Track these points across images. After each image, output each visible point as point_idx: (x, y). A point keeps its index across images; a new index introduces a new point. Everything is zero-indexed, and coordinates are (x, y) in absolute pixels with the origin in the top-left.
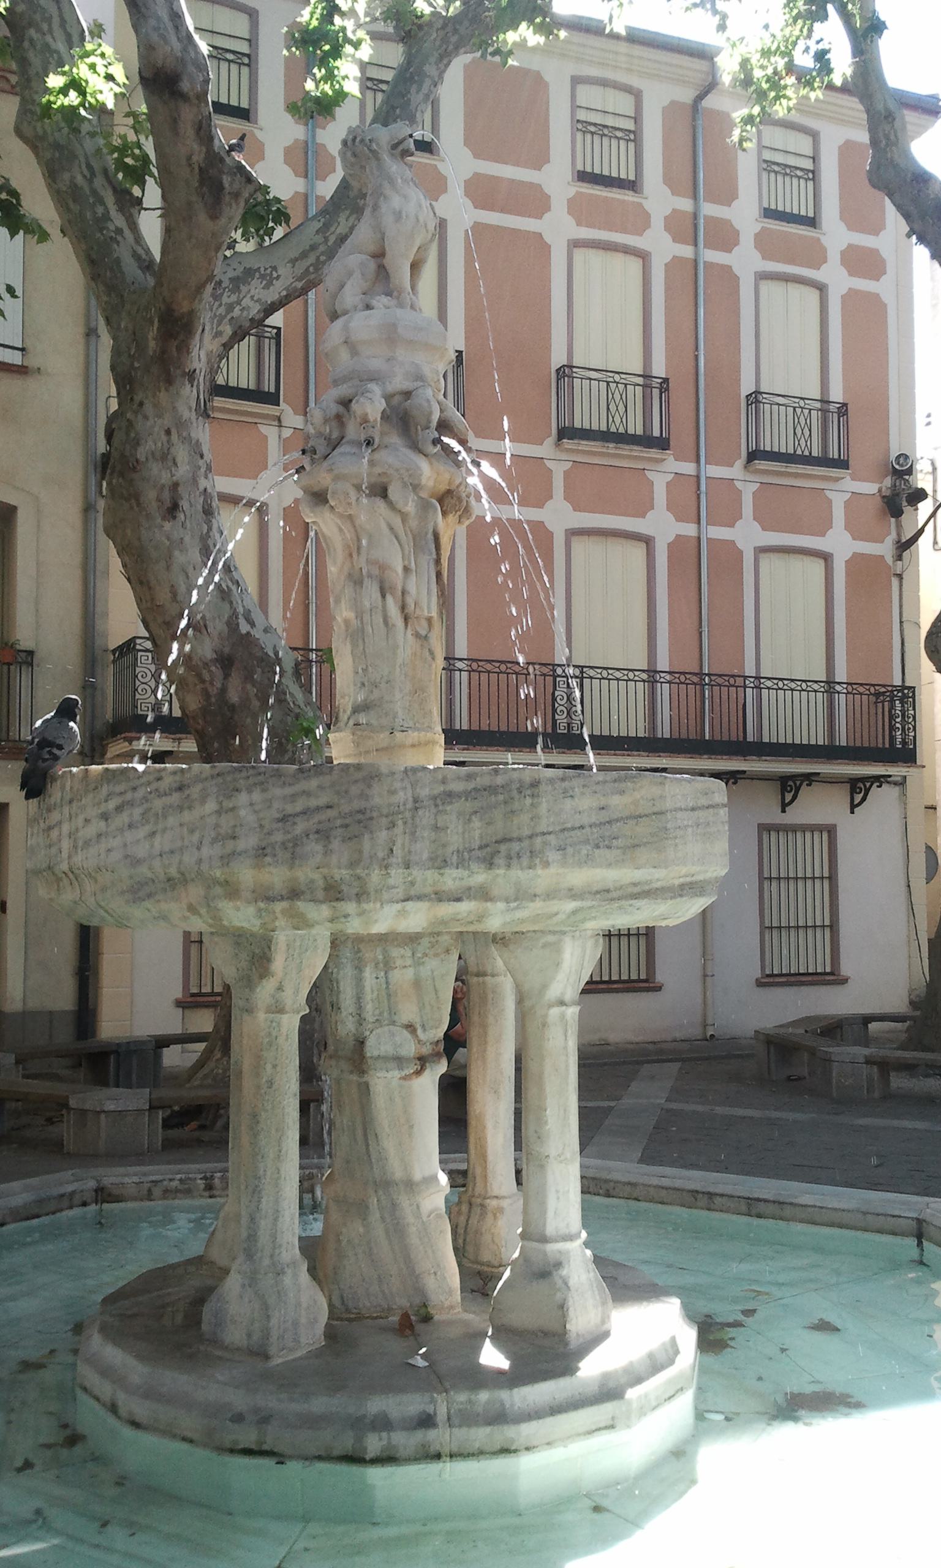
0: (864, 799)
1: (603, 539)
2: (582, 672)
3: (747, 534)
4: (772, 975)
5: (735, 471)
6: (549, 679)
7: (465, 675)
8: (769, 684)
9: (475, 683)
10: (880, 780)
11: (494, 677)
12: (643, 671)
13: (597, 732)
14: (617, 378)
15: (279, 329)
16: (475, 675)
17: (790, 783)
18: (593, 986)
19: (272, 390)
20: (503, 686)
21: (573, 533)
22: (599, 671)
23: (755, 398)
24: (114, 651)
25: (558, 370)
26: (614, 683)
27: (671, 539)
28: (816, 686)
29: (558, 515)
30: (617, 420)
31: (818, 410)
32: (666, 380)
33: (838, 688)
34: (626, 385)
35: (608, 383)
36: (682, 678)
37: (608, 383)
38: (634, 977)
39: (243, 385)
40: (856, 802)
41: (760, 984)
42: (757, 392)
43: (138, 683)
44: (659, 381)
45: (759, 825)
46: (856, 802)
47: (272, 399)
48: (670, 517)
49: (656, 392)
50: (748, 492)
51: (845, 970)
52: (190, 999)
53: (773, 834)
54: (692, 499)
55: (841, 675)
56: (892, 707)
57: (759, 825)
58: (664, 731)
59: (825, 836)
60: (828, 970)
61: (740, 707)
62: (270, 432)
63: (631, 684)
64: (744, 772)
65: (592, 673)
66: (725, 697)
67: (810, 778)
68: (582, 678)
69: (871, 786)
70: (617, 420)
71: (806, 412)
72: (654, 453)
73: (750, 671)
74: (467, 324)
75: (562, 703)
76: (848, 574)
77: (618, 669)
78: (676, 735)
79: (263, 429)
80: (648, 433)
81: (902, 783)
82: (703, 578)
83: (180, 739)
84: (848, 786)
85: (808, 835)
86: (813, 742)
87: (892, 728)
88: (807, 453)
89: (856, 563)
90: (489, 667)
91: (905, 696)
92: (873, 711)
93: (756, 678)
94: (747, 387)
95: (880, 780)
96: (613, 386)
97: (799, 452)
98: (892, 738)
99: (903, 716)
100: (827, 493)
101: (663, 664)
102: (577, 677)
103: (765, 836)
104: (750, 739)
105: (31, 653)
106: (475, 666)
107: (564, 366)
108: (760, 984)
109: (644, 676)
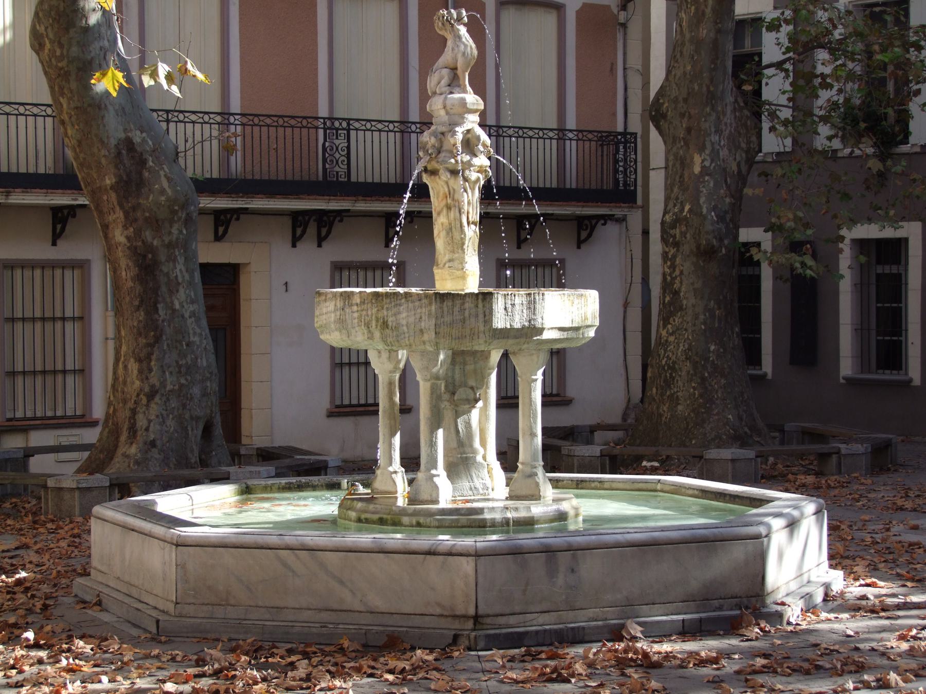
0: (590, 235)
2: (349, 124)
4: (342, 406)
7: (574, 143)
8: (511, 132)
10: (606, 218)
11: (198, 126)
12: (551, 130)
13: (535, 185)
17: (325, 218)
18: (506, 401)
22: (364, 123)
26: (31, 119)
28: (551, 134)
36: (521, 133)
38: (354, 402)
40: (583, 237)
41: (331, 414)
45: (332, 262)
46: (583, 237)
51: (571, 392)
52: (7, 424)
53: (18, 272)
55: (571, 123)
56: (617, 151)
57: (332, 262)
58: (571, 182)
60: (555, 392)
64: (348, 211)
65: (357, 125)
66: (265, 137)
67: (340, 214)
68: (348, 131)
69: (596, 224)
73: (323, 112)
75: (343, 153)
78: (581, 186)
81: (622, 220)
83: (10, 192)
86: (548, 185)
87: (616, 171)
90: (268, 121)
91: (626, 142)
92: (599, 153)
93: (401, 122)
95: (606, 218)
98: (617, 181)
99: (625, 160)
101: (236, 106)
102: (344, 129)
104: (354, 179)
108: (331, 414)
109: (219, 119)
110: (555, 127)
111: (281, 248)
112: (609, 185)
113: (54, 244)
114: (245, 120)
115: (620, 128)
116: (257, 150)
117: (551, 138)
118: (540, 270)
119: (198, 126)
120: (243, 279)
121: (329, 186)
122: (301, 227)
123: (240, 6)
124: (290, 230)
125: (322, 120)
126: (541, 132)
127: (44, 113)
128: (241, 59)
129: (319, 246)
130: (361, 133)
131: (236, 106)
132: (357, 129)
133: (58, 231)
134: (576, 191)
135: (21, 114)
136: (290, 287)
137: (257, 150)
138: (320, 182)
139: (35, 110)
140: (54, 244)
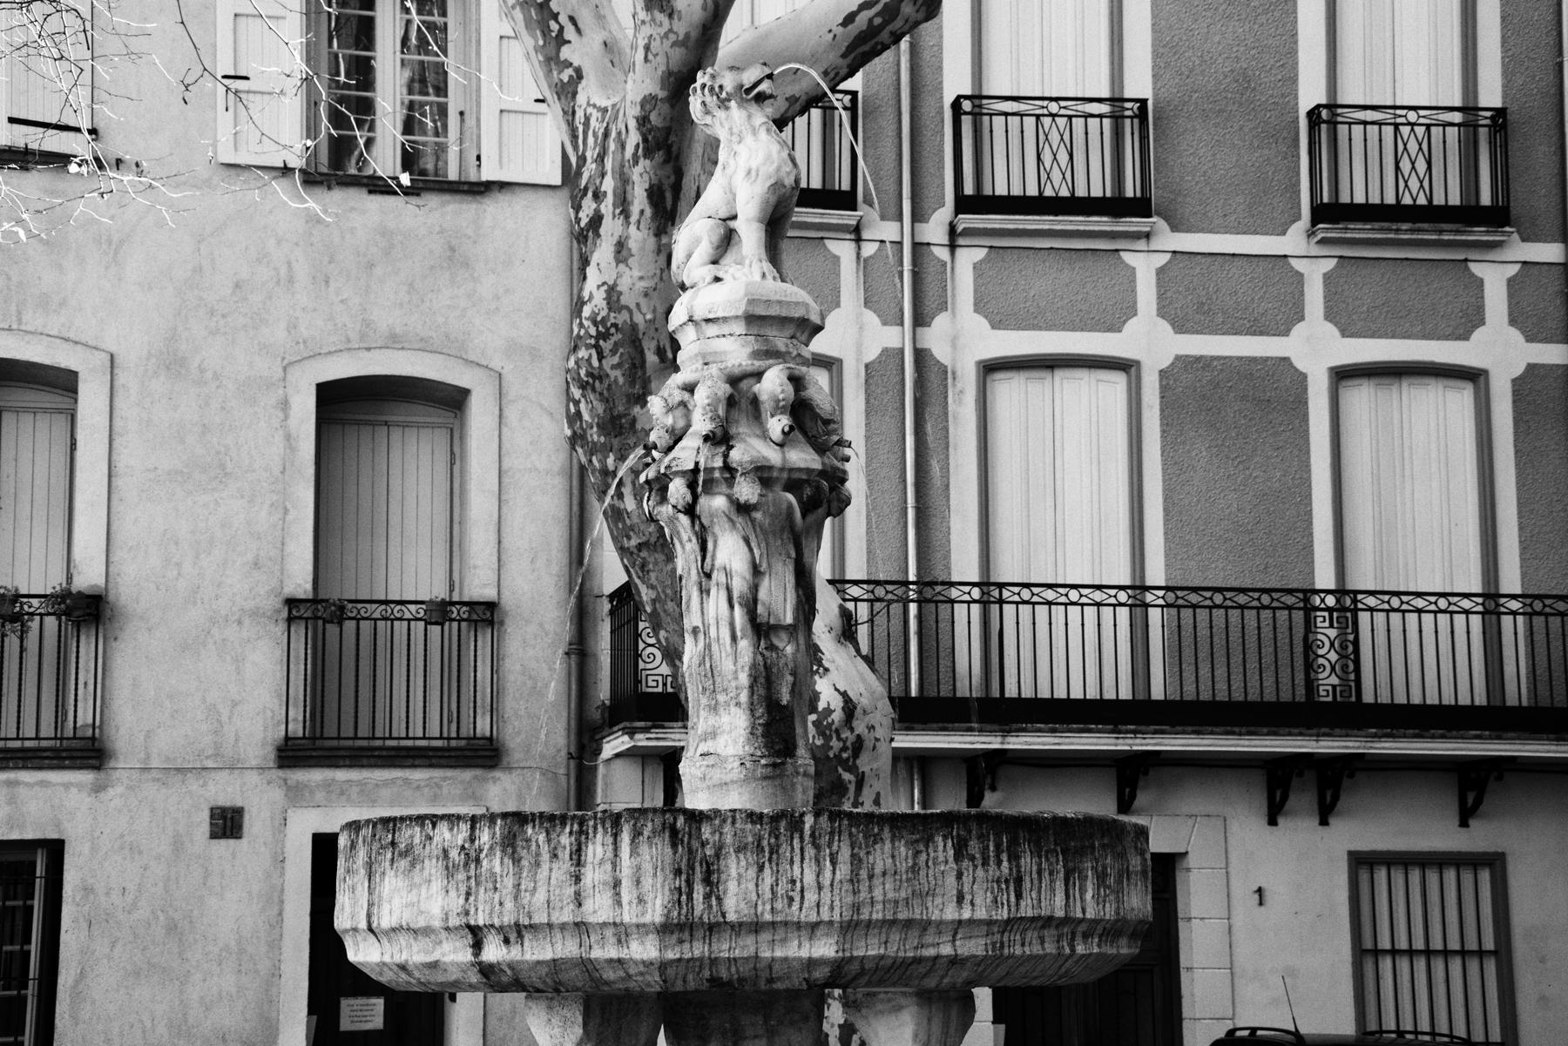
1: (1046, 374)
2: (1355, 601)
3: (1315, 347)
5: (1293, 241)
6: (1298, 616)
8: (1371, 601)
9: (1540, 637)
14: (1412, 116)
15: (1143, 102)
16: (1539, 621)
19: (846, 186)
20: (1267, 631)
21: (1343, 375)
22: (1112, 592)
23: (1326, 118)
24: (611, 597)
25: (1310, 114)
26: (1042, 611)
27: (1519, 370)
28: (1466, 604)
29: (1315, 347)
30: (1414, 184)
31: (1459, 125)
32: (1500, 113)
33: (1149, 597)
34: (1070, 117)
35: (1396, 126)
36: (1395, 602)
37: (1396, 126)
39: (1096, 192)
42: (1332, 106)
43: (641, 645)
44: (1488, 114)
45: (1350, 853)
47: (846, 200)
48: (1515, 335)
49: (1483, 132)
50: (1315, 273)
54: (1193, 296)
55: (1511, 581)
57: (1350, 853)
58: (1516, 691)
59: (1485, 876)
61: (1299, 649)
62: (843, 249)
63: (1074, 611)
68: (1355, 611)
70: (1414, 184)
71: (1420, 131)
72: (1479, 234)
73: (1324, 578)
74: (1156, 55)
76: (1164, 390)
77: (1099, 587)
79: (835, 247)
80: (828, 187)
82: (1231, 420)
84: (1114, 770)
85: (1415, 876)
88: (1422, 201)
89: (1528, 384)
94: (1311, 93)
96: (1405, 130)
97: (1407, 200)
100: (1474, 267)
101: (1156, 574)
103: (1364, 876)
104: (1368, 698)
105: (491, 606)
106: (1538, 606)
107: (1319, 106)
110: (1477, 589)
111: (1246, 825)
112: (1290, 690)
113: (1464, 824)
114: (1171, 597)
115: (1324, 578)
116: (1268, 650)
117: (1467, 612)
118: (1467, 877)
119: (1250, 615)
120: (1180, 877)
121: (1305, 714)
122: (1280, 787)
123: (1162, 410)
124: (1456, 799)
125: (1301, 596)
126: (1445, 602)
127: (1113, 601)
128: (1166, 499)
129: (1272, 822)
130: (1380, 618)
131: (1156, 574)
132: (1371, 610)
133: (1328, 799)
134: (1165, 704)
135: (1024, 602)
136: (1268, 896)
137: (1268, 650)
138: (1300, 703)
139: (1194, 598)
140: (1464, 824)
